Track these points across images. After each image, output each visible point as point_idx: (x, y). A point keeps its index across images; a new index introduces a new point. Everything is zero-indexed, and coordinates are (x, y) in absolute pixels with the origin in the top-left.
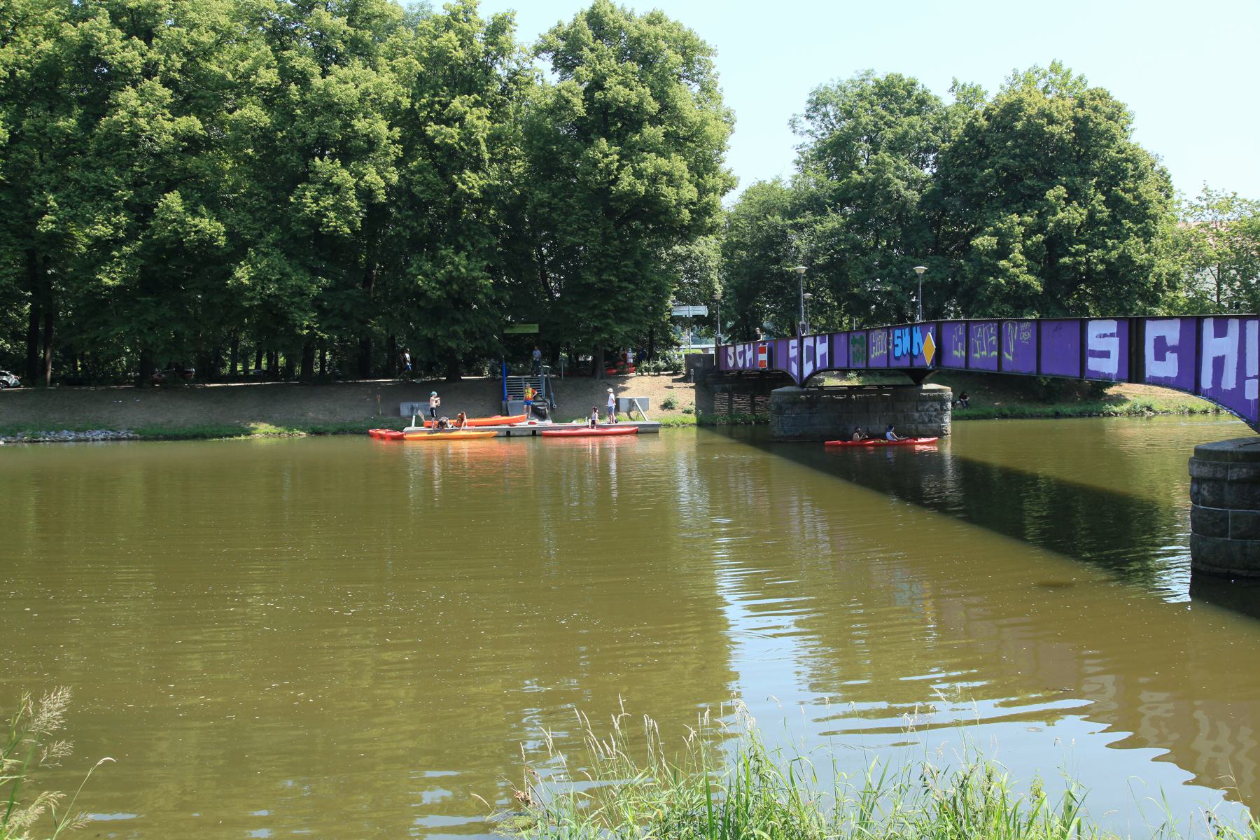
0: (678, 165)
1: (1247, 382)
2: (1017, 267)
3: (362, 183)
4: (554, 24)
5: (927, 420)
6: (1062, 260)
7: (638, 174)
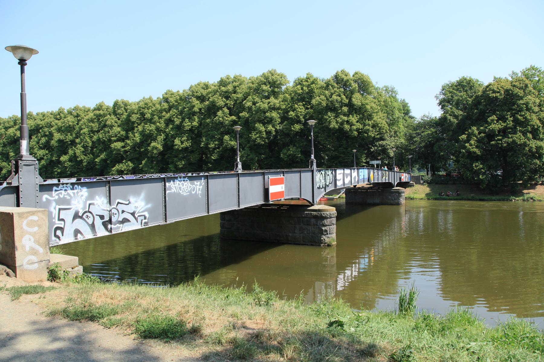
0: (354, 119)
5: (394, 199)
6: (491, 143)
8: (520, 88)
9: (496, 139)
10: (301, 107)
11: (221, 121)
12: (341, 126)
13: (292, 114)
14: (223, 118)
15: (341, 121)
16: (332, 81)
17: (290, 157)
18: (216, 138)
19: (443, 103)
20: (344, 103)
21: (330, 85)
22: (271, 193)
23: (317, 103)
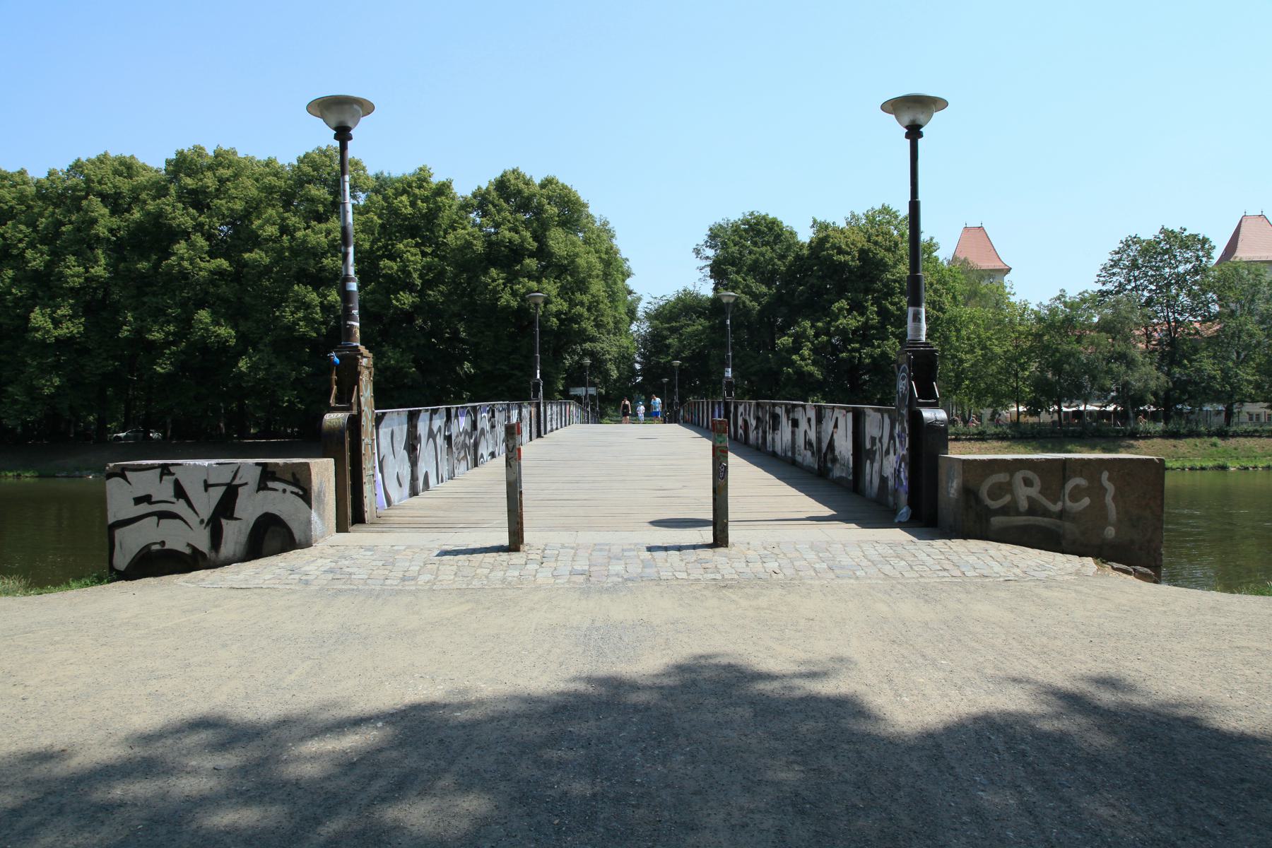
0: (550, 287)
1: (706, 446)
2: (805, 360)
3: (325, 302)
4: (474, 188)
6: (841, 355)
7: (514, 294)
8: (888, 250)
9: (850, 347)
10: (412, 250)
11: (186, 269)
12: (523, 303)
13: (389, 266)
14: (191, 261)
15: (523, 291)
16: (494, 194)
17: (388, 373)
18: (170, 314)
19: (718, 271)
20: (528, 250)
21: (490, 202)
22: (307, 465)
23: (458, 243)
